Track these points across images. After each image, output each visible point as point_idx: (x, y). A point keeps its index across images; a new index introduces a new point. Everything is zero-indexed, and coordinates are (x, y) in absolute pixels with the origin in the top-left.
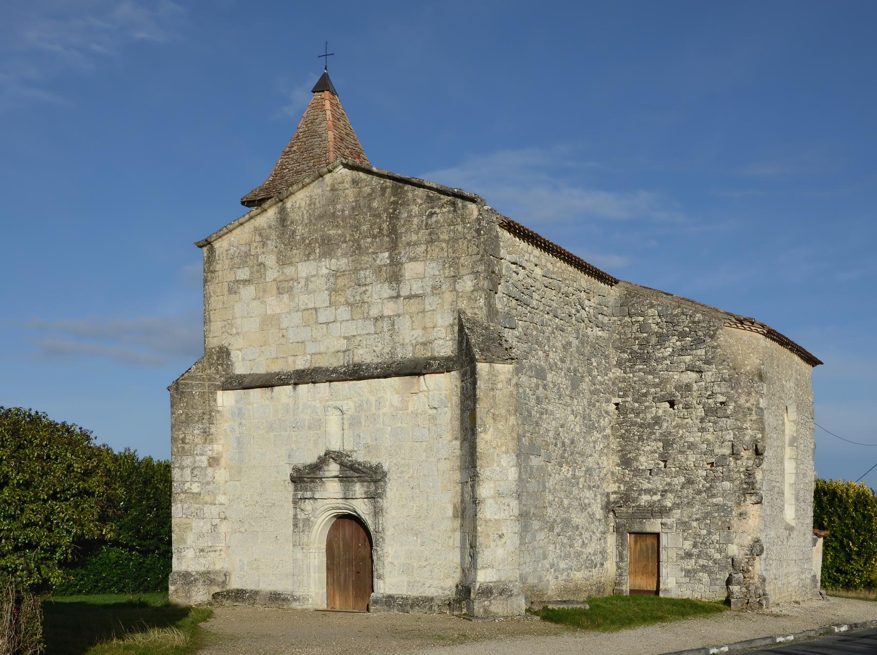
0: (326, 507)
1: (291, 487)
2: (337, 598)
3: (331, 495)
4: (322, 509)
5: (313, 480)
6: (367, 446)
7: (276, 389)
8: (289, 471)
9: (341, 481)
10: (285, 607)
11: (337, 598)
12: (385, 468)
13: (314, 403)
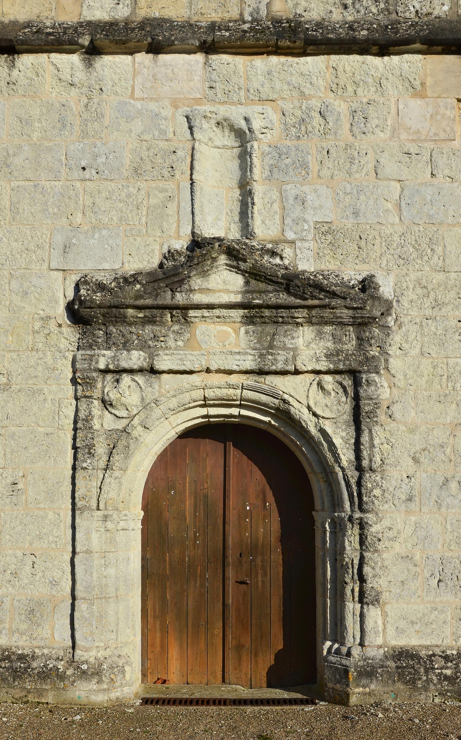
0: (186, 397)
1: (69, 335)
2: (174, 653)
3: (211, 359)
4: (174, 403)
5: (154, 313)
6: (325, 230)
7: (26, 60)
8: (64, 292)
9: (249, 320)
10: (50, 698)
11: (174, 653)
12: (386, 289)
13: (153, 106)
